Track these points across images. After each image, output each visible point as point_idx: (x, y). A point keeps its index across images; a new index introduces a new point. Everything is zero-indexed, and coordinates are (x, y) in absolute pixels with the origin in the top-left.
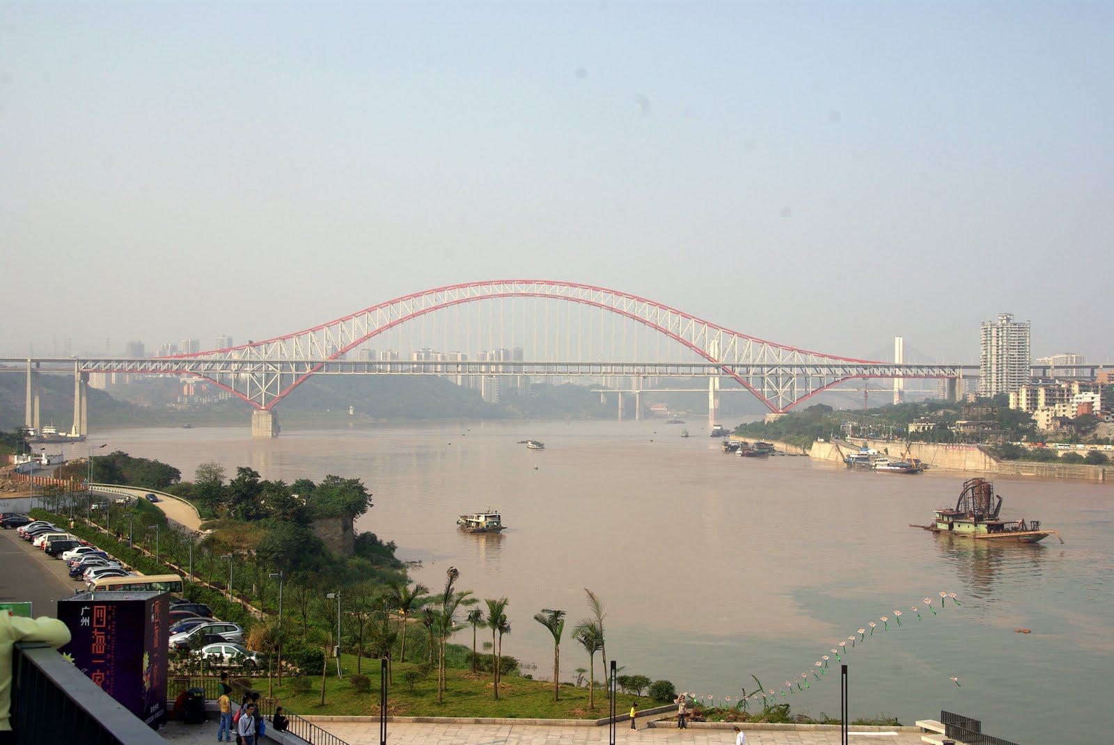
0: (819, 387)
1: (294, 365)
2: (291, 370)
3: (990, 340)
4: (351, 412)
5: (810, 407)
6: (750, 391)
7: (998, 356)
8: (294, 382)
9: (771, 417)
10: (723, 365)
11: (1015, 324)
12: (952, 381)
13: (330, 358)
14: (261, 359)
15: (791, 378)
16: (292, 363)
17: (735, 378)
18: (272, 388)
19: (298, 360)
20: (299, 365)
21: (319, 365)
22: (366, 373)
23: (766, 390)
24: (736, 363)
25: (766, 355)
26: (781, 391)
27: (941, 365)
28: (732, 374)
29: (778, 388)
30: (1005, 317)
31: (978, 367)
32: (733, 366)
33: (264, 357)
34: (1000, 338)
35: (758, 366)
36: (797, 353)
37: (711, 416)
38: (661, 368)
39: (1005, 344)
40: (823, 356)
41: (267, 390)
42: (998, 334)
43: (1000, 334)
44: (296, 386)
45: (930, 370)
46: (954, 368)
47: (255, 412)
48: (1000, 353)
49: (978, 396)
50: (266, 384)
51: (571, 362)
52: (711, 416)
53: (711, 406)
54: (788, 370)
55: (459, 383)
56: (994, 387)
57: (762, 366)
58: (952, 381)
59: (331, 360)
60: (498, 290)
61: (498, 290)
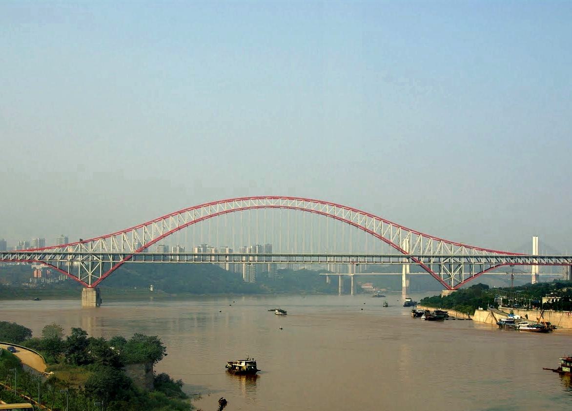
2: (109, 260)
4: (152, 289)
9: (446, 293)
10: (412, 256)
14: (88, 252)
15: (460, 265)
17: (420, 265)
18: (96, 273)
19: (114, 252)
20: (115, 256)
21: (129, 256)
23: (442, 273)
25: (442, 249)
26: (453, 274)
32: (419, 257)
33: (90, 251)
37: (404, 292)
40: (482, 250)
41: (92, 274)
44: (113, 271)
47: (84, 289)
50: (91, 270)
52: (404, 292)
53: (404, 285)
54: (458, 260)
55: (227, 269)
57: (439, 257)
59: (138, 253)
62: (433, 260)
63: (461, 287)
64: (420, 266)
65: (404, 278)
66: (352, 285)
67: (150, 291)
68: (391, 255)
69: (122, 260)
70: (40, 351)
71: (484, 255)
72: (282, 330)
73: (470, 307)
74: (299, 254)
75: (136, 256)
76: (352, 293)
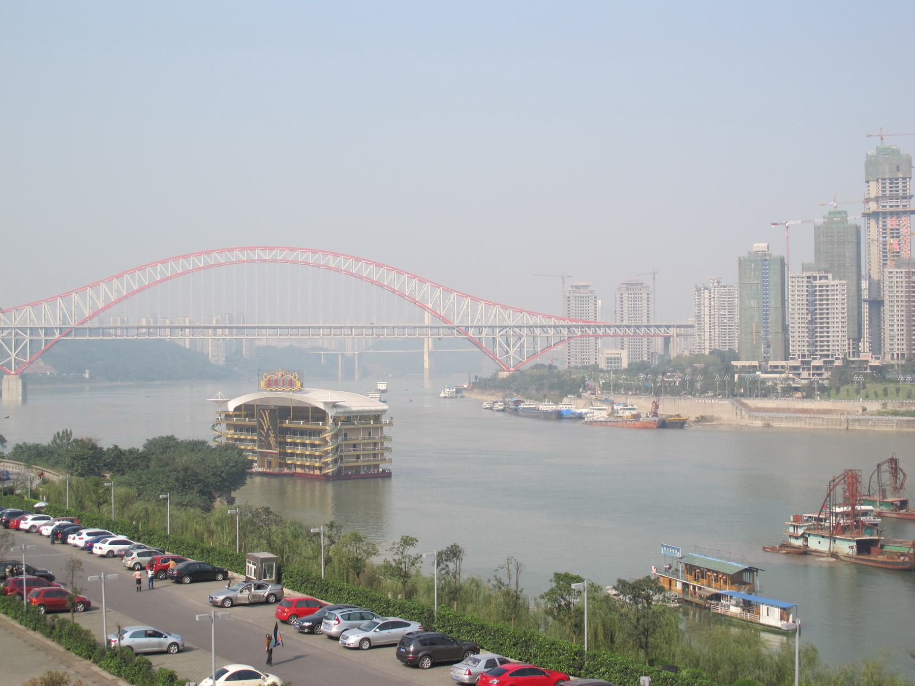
0: (546, 347)
1: (43, 330)
2: (40, 335)
3: (704, 343)
4: (87, 376)
5: (535, 366)
6: (483, 351)
7: (710, 316)
8: (43, 347)
9: (504, 375)
10: (457, 327)
11: (725, 287)
12: (667, 340)
13: (79, 324)
14: (11, 325)
15: (520, 338)
16: (41, 328)
17: (469, 339)
18: (22, 353)
19: (47, 325)
20: (48, 331)
21: (67, 331)
22: (101, 337)
23: (497, 349)
24: (470, 324)
25: (495, 316)
26: (512, 352)
27: (656, 324)
28: (465, 335)
29: (509, 347)
30: (716, 281)
31: (693, 327)
32: (467, 327)
33: (15, 324)
34: (712, 308)
35: (490, 327)
36: (526, 314)
37: (426, 375)
38: (346, 330)
39: (716, 305)
40: (550, 317)
41: (16, 355)
42: (711, 296)
43: (712, 304)
44: (45, 351)
45: (607, 329)
46: (668, 327)
47: (5, 377)
48: (712, 313)
49: (692, 353)
50: (15, 352)
51: (271, 325)
52: (426, 375)
53: (426, 365)
54: (517, 330)
55: (187, 346)
56: (707, 344)
57: (493, 327)
58: (667, 340)
59: (80, 326)
60: (218, 257)
61: (218, 257)
62: (485, 331)
63: (523, 368)
64: (467, 340)
65: (426, 357)
66: (356, 366)
67: (85, 378)
68: (278, 325)
69: (57, 336)
70: (15, 449)
71: (552, 324)
72: (393, 416)
73: (557, 392)
74: (273, 325)
75: (129, 330)
76: (356, 377)
